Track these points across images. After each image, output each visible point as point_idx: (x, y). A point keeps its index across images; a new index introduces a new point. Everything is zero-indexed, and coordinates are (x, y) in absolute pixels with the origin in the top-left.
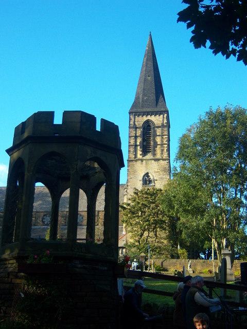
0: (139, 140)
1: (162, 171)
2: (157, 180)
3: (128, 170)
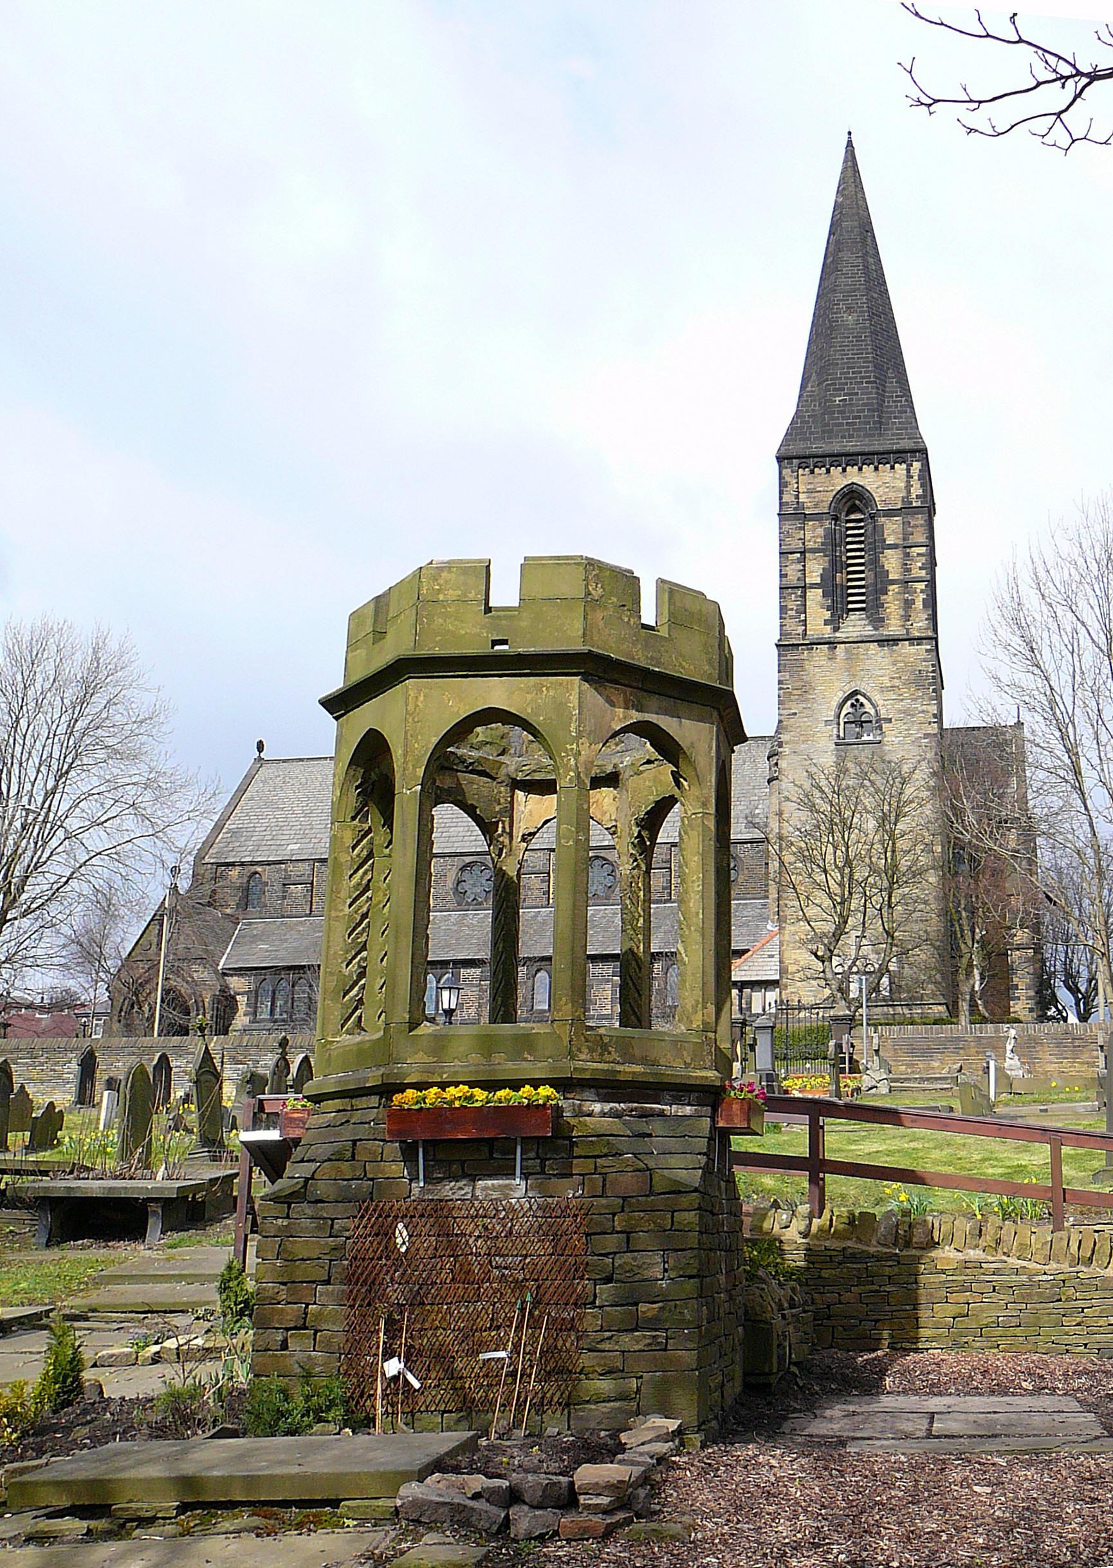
0: (815, 569)
1: (907, 683)
2: (890, 720)
3: (780, 682)
